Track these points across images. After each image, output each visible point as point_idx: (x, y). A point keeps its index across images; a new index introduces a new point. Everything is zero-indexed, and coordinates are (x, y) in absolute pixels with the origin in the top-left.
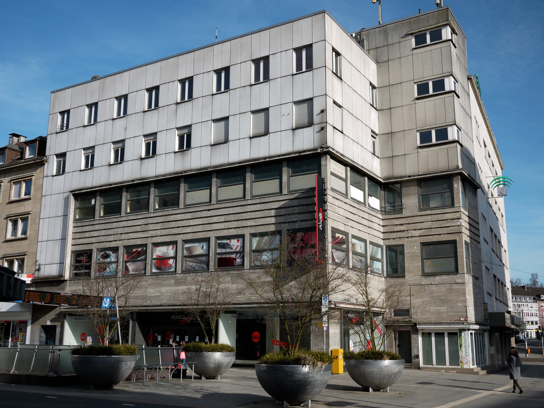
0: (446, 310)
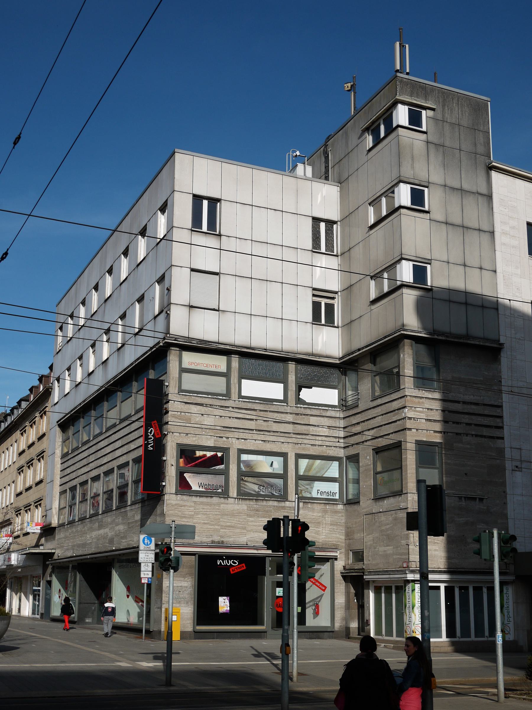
0: (392, 552)
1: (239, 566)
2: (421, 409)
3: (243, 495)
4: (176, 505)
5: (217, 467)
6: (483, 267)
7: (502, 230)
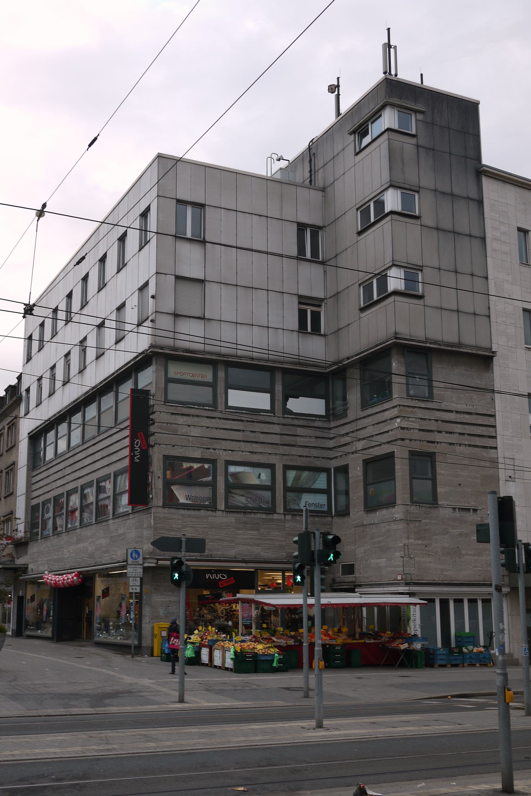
1: (227, 580)
2: (414, 419)
3: (230, 509)
4: (164, 518)
5: (205, 479)
6: (475, 273)
7: (493, 235)
